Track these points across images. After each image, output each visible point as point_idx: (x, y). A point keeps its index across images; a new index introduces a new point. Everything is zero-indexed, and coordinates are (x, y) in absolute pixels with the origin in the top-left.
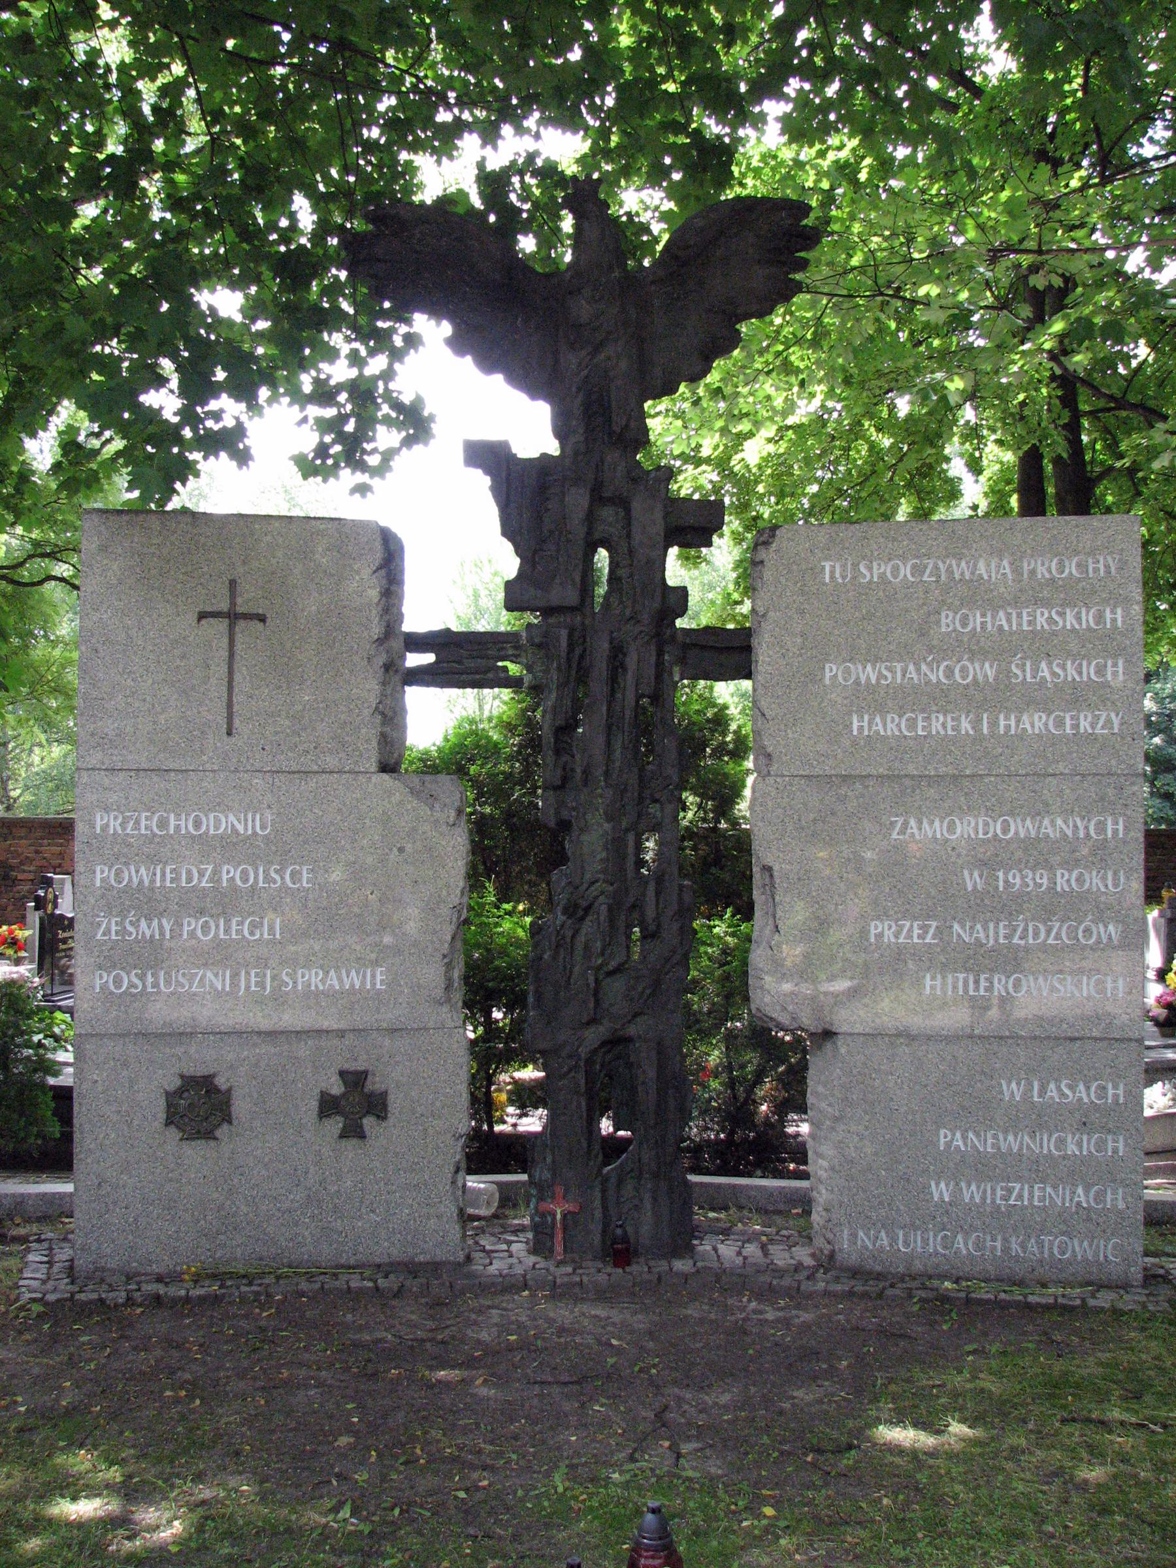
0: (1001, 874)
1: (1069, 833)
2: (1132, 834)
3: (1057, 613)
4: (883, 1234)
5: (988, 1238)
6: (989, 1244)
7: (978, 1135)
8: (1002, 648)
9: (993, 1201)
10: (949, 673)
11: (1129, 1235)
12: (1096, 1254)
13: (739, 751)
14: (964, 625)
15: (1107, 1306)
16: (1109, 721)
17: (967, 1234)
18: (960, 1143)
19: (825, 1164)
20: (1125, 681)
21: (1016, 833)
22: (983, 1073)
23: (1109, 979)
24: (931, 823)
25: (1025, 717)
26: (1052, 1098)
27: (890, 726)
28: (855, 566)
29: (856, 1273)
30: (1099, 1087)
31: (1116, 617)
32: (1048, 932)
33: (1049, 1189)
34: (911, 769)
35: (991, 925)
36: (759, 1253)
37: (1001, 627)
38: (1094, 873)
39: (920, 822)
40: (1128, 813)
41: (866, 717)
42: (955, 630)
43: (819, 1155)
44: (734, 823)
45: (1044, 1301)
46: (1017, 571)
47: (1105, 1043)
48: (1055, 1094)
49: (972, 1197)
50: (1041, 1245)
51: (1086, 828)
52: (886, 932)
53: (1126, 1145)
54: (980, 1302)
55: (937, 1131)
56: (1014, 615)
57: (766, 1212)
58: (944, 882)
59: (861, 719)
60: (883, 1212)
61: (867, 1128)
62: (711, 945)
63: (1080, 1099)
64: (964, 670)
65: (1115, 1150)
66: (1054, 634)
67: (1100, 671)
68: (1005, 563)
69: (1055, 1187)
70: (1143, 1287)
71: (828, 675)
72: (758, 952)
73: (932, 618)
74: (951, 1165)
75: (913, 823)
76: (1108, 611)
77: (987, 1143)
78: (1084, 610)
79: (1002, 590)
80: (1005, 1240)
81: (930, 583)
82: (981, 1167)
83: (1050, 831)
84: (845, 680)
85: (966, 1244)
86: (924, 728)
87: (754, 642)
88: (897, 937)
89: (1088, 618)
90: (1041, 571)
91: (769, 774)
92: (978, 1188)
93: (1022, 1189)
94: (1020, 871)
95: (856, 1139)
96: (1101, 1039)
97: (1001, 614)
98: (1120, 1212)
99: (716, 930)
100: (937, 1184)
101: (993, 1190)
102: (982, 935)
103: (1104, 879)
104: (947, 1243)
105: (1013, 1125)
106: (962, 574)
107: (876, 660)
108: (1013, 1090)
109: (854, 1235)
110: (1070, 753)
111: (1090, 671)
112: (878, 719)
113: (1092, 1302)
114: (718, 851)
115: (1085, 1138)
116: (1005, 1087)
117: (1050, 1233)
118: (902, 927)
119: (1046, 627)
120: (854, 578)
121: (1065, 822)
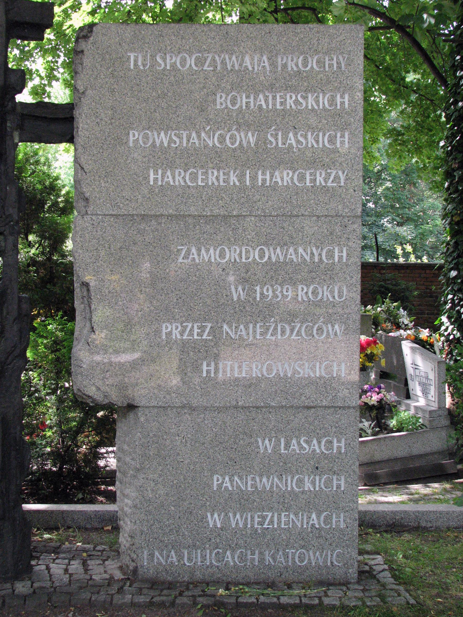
0: (258, 288)
1: (308, 258)
2: (352, 259)
3: (302, 96)
4: (173, 553)
5: (249, 552)
6: (249, 557)
7: (241, 478)
8: (260, 122)
9: (252, 526)
10: (222, 139)
11: (348, 546)
12: (325, 561)
13: (66, 210)
14: (233, 104)
15: (337, 603)
16: (337, 178)
17: (233, 551)
18: (229, 485)
19: (129, 502)
20: (350, 148)
21: (270, 258)
22: (245, 433)
23: (335, 365)
24: (208, 251)
25: (277, 173)
26: (294, 450)
27: (177, 178)
28: (153, 57)
29: (154, 584)
30: (327, 442)
31: (344, 101)
32: (292, 331)
33: (292, 516)
34: (193, 210)
35: (251, 326)
36: (81, 570)
37: (260, 106)
38: (325, 288)
39: (199, 250)
40: (350, 244)
41: (160, 172)
42: (227, 107)
43: (126, 496)
44: (63, 256)
45: (292, 601)
46: (273, 65)
47: (332, 409)
48: (296, 447)
49: (237, 523)
50: (286, 556)
51: (320, 255)
52: (174, 331)
53: (346, 482)
54: (246, 605)
55: (212, 476)
56: (270, 98)
57: (86, 529)
58: (217, 294)
59: (156, 173)
60: (172, 537)
61: (160, 476)
62: (46, 338)
63: (314, 450)
64: (233, 138)
65: (339, 486)
66: (300, 112)
67: (332, 140)
68: (265, 58)
69: (296, 514)
70: (358, 583)
71: (131, 138)
72: (79, 347)
73: (210, 98)
74: (222, 500)
75: (194, 250)
76: (338, 96)
77: (247, 484)
78: (321, 96)
79: (262, 78)
80: (260, 553)
81: (209, 72)
82: (243, 502)
83: (294, 257)
84: (144, 143)
85: (233, 558)
86: (203, 180)
87: (76, 113)
88: (182, 335)
89: (324, 101)
90: (291, 65)
91: (87, 213)
92: (241, 517)
93: (273, 516)
94: (272, 286)
95: (153, 484)
96: (329, 407)
97: (261, 96)
98: (341, 530)
99: (49, 327)
100: (212, 515)
101: (252, 518)
102: (244, 333)
103: (332, 292)
104: (220, 557)
105: (265, 471)
106: (233, 66)
107: (167, 129)
108: (266, 445)
109: (152, 555)
110: (309, 200)
111: (324, 140)
112: (169, 173)
113: (326, 601)
114: (51, 272)
115: (317, 478)
116: (260, 444)
117: (293, 547)
118: (185, 328)
119: (293, 106)
120: (152, 66)
121: (305, 250)
